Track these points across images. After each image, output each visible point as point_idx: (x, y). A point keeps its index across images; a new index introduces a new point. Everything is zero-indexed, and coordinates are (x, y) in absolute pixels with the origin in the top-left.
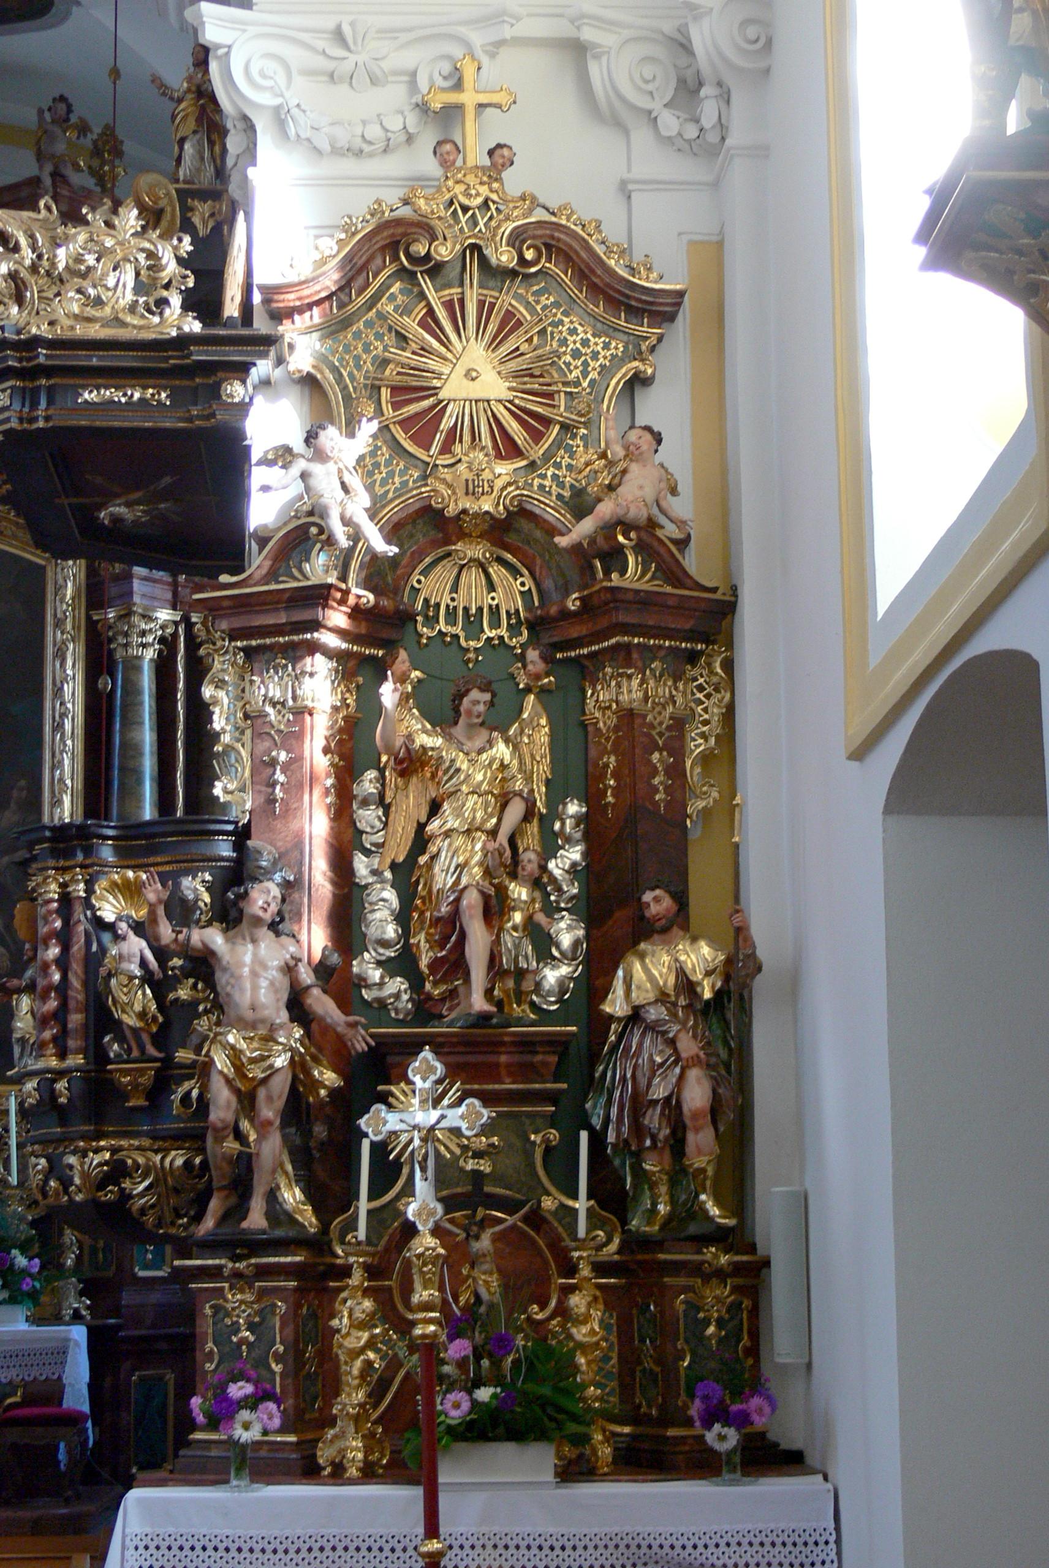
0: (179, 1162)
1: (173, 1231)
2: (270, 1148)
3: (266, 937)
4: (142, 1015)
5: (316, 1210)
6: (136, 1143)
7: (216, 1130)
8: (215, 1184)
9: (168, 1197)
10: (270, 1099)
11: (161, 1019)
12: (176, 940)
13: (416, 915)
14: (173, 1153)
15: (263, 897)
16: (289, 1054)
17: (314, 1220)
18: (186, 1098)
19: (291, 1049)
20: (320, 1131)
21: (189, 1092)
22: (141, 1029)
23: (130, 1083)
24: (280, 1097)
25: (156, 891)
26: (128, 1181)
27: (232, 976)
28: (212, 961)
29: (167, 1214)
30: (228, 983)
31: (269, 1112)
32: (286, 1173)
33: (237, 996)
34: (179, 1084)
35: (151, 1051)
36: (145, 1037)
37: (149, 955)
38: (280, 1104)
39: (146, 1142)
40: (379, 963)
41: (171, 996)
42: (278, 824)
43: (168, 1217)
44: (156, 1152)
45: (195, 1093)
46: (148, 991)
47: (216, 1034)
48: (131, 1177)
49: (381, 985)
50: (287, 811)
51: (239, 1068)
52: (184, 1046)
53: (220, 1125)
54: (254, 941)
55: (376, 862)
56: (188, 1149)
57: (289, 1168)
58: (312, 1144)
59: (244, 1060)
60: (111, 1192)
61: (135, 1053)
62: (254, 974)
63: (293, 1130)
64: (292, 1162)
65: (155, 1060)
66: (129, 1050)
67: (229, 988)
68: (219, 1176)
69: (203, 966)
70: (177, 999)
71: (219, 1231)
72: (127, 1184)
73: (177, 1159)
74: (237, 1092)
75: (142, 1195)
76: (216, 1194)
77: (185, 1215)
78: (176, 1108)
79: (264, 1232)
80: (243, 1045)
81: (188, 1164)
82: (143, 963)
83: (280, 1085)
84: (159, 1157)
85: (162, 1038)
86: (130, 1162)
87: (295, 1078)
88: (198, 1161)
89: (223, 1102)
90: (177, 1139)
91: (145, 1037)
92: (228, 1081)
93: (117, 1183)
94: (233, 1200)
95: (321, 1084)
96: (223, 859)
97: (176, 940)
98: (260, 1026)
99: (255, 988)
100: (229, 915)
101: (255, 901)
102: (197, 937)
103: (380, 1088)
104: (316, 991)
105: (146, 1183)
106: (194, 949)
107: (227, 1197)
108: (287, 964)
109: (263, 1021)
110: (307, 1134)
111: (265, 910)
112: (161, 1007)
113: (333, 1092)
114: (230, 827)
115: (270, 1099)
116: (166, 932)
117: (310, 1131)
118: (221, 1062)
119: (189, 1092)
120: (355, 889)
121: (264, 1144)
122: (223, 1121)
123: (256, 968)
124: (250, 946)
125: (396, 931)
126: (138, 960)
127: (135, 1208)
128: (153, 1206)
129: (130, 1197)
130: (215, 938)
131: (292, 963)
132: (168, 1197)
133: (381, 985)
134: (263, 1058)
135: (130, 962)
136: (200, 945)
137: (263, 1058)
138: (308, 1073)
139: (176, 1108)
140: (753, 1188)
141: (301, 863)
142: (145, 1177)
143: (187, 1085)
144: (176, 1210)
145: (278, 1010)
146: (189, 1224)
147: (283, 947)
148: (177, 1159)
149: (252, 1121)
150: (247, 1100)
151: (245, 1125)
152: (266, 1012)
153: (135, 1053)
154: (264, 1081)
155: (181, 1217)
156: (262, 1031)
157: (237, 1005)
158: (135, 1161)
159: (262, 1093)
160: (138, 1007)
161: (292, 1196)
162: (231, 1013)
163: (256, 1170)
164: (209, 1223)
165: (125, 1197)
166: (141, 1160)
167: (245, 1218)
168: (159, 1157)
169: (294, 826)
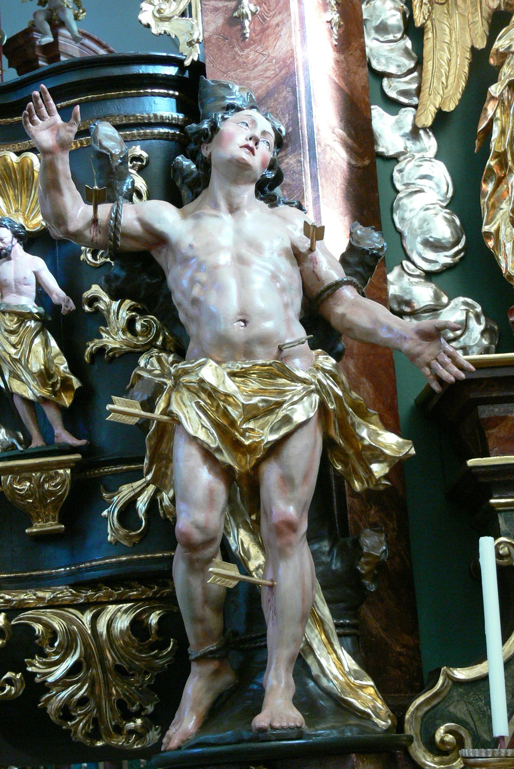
0: (123, 623)
1: (119, 741)
2: (294, 576)
3: (254, 211)
4: (45, 376)
5: (382, 688)
6: (48, 595)
7: (191, 547)
8: (194, 651)
9: (107, 685)
10: (288, 481)
11: (76, 383)
12: (95, 221)
13: (488, 187)
14: (112, 608)
15: (243, 135)
16: (316, 397)
17: (379, 703)
18: (128, 510)
19: (321, 389)
20: (374, 544)
21: (132, 502)
22: (45, 400)
23: (30, 493)
24: (306, 477)
25: (53, 127)
26: (37, 660)
27: (200, 266)
28: (161, 257)
29: (108, 715)
30: (193, 282)
31: (288, 503)
32: (321, 622)
33: (212, 300)
34: (114, 490)
35: (64, 437)
36: (52, 415)
37: (51, 282)
38: (306, 490)
39: (65, 593)
40: (429, 276)
41: (92, 346)
42: (251, 54)
43: (110, 718)
44: (82, 608)
45: (142, 505)
46: (53, 343)
47: (177, 377)
48: (45, 655)
49: (434, 310)
50: (263, 30)
51: (226, 429)
52: (124, 393)
53: (197, 537)
54: (233, 209)
55: (407, 116)
56: (136, 600)
57: (325, 611)
58: (363, 568)
59: (234, 413)
60: (9, 681)
61: (37, 442)
62: (241, 260)
63: (325, 546)
64: (329, 602)
65: (72, 450)
66: (28, 441)
67: (196, 291)
68: (200, 629)
69: (143, 270)
70: (102, 350)
71: (210, 737)
72: (36, 667)
73: (119, 618)
74: (226, 474)
75: (63, 683)
76: (195, 668)
77: (138, 715)
78: (113, 530)
79: (299, 733)
80: (230, 386)
81: (138, 626)
82: (42, 295)
83: (304, 453)
84: (87, 618)
85: (82, 412)
86: (38, 628)
87: (329, 444)
88: (154, 619)
89: (198, 491)
90: (117, 583)
91: (52, 415)
92: (208, 455)
93: (20, 667)
94: (228, 678)
95: (377, 455)
96: (162, 124)
97: (95, 221)
98: (259, 350)
99: (244, 283)
100: (185, 181)
101: (231, 137)
102: (130, 215)
103: (471, 462)
104: (348, 293)
105: (70, 662)
106: (126, 236)
107: (216, 673)
108: (294, 248)
109: (264, 340)
110: (352, 551)
111: (252, 150)
112: (76, 365)
113: (399, 467)
114: (171, 71)
115: (288, 481)
116: (78, 212)
117: (357, 544)
118: (194, 421)
119: (132, 502)
120: (379, 163)
121: (282, 565)
122: (202, 529)
123: (243, 260)
124: (227, 218)
125: (451, 222)
126: (32, 289)
127: (53, 707)
128: (83, 702)
129: (44, 688)
130: (165, 216)
131: (304, 244)
132: (107, 685)
133: (434, 310)
134: (271, 408)
135: (19, 293)
136: (137, 227)
137: (271, 408)
138: (349, 433)
139: (113, 530)
140: (478, 677)
141: (295, 106)
142: (67, 650)
143: (126, 491)
144: (121, 704)
145: (288, 321)
146: (146, 728)
147: (284, 219)
148: (119, 618)
149: (255, 531)
150: (245, 493)
151: (242, 539)
152: (269, 325)
153: (37, 442)
154: (275, 449)
155: (130, 717)
156: (264, 358)
157: (213, 317)
158: (47, 626)
159: (271, 474)
160: (37, 364)
161: (337, 665)
162: (200, 333)
163: (268, 615)
164: (186, 724)
165: (36, 688)
166: (57, 624)
167: (258, 710)
168: (87, 618)
169: (278, 48)
